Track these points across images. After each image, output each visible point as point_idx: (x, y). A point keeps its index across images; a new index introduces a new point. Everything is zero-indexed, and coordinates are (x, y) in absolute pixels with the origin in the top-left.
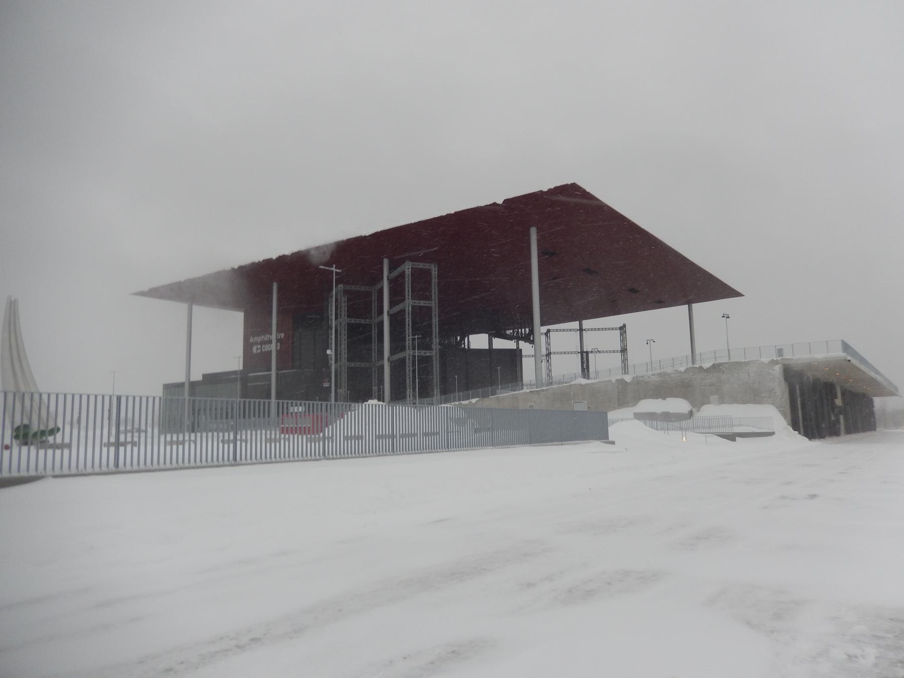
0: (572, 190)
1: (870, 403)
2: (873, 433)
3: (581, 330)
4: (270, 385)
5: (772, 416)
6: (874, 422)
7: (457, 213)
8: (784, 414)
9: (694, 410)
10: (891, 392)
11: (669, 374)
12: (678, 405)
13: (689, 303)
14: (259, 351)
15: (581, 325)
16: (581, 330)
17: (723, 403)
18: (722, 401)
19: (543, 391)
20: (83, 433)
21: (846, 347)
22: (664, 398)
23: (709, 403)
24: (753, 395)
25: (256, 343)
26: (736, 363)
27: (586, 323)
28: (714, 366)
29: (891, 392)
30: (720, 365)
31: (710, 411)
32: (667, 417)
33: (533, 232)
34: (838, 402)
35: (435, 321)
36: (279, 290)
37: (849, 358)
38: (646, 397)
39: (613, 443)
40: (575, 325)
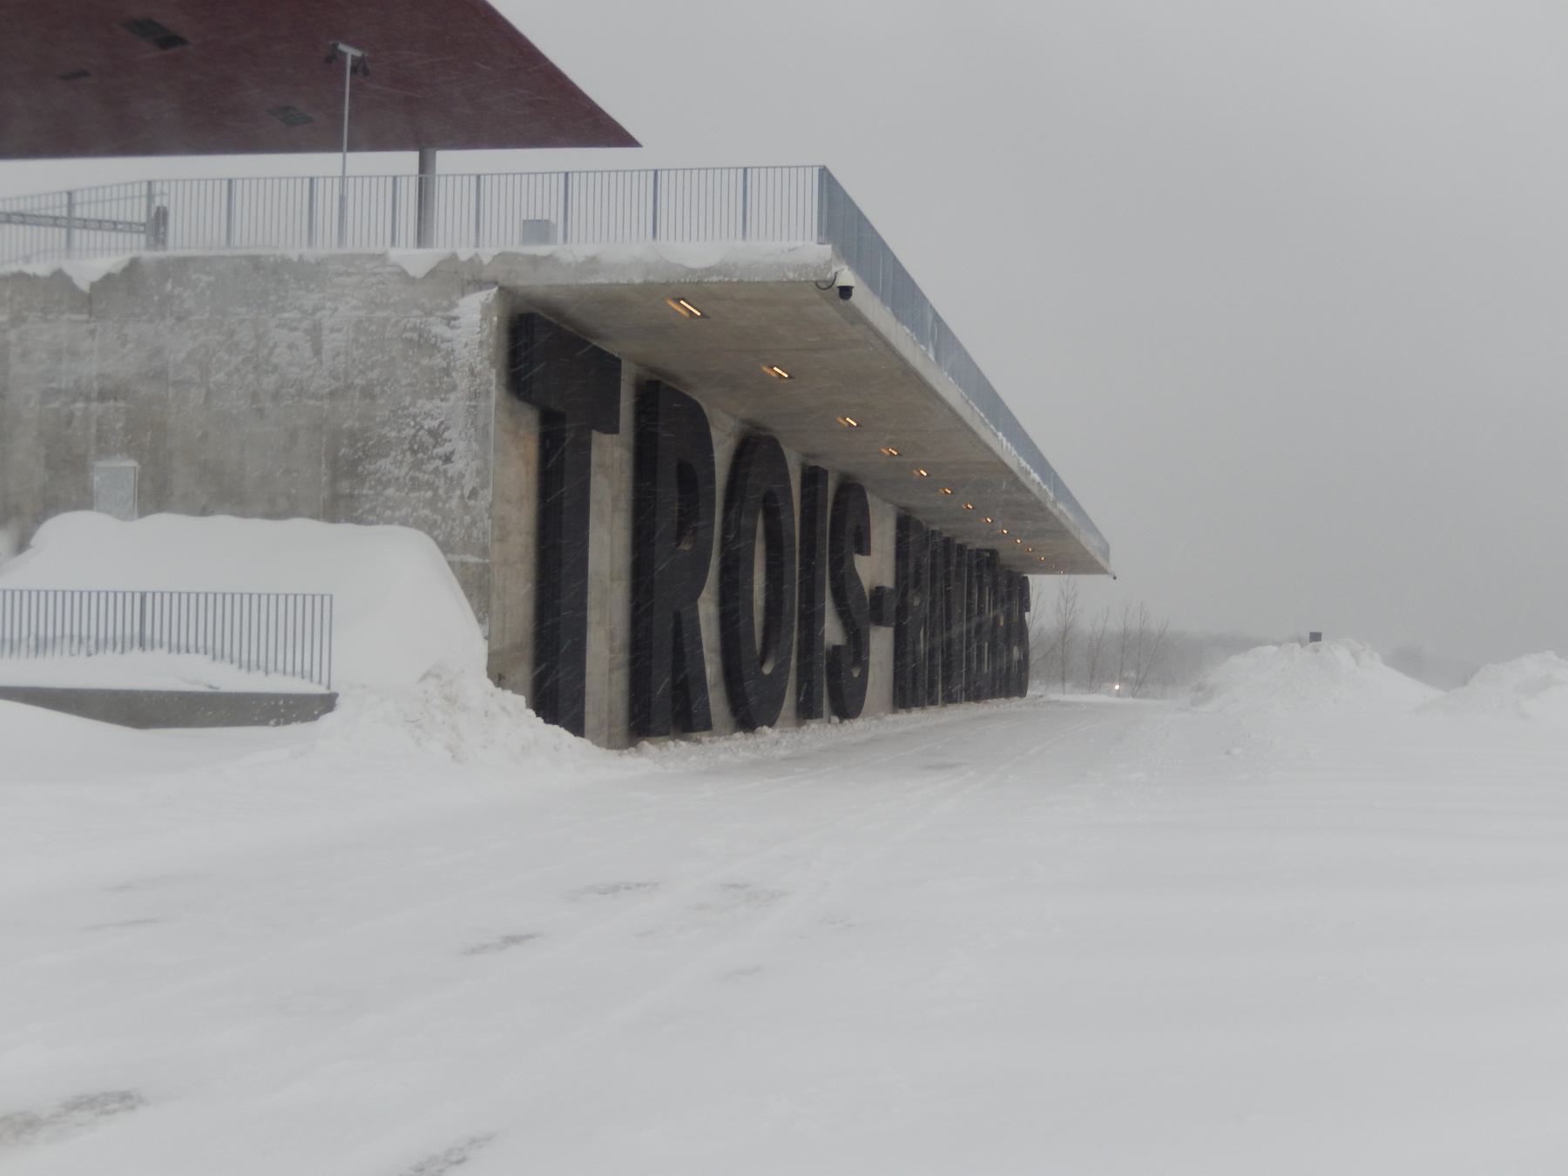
1: (1017, 594)
2: (1016, 700)
5: (404, 608)
6: (1024, 664)
10: (1076, 560)
13: (424, 142)
18: (155, 495)
20: (33, 630)
21: (839, 216)
23: (84, 500)
24: (341, 478)
26: (256, 263)
28: (130, 276)
29: (1076, 560)
34: (875, 568)
37: (847, 277)
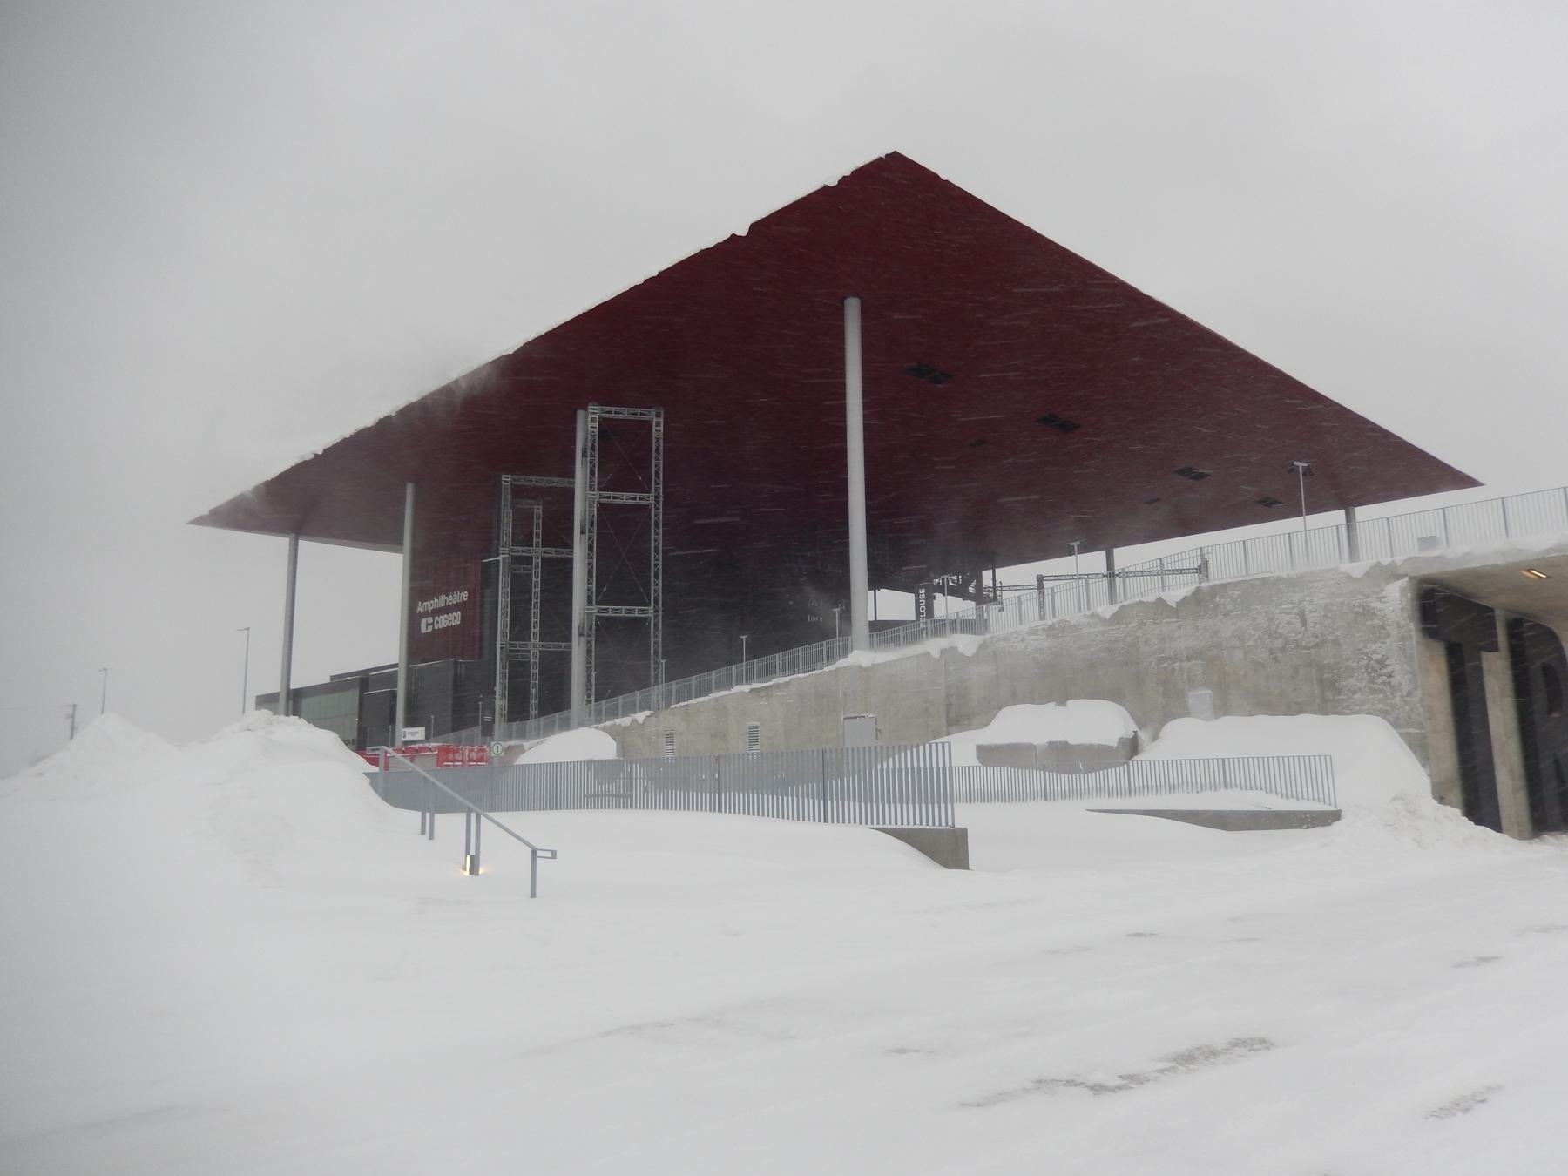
0: (895, 162)
3: (1111, 574)
4: (394, 695)
8: (1420, 747)
9: (1144, 736)
11: (1076, 628)
12: (1097, 722)
14: (430, 629)
17: (1225, 714)
18: (1223, 707)
19: (778, 686)
22: (1062, 702)
23: (1186, 713)
25: (426, 614)
30: (1215, 591)
31: (1192, 739)
33: (852, 308)
35: (657, 537)
36: (417, 495)
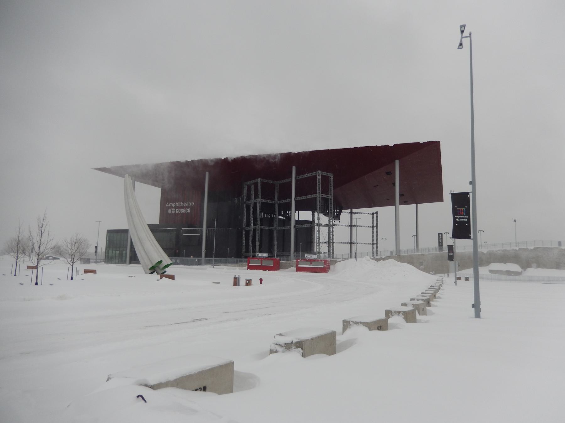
7: (361, 148)
12: (514, 267)
13: (416, 202)
14: (173, 212)
15: (351, 211)
16: (351, 213)
22: (505, 263)
23: (531, 267)
25: (171, 207)
27: (354, 210)
28: (535, 249)
30: (538, 248)
32: (509, 273)
38: (494, 262)
39: (456, 284)
40: (349, 211)
